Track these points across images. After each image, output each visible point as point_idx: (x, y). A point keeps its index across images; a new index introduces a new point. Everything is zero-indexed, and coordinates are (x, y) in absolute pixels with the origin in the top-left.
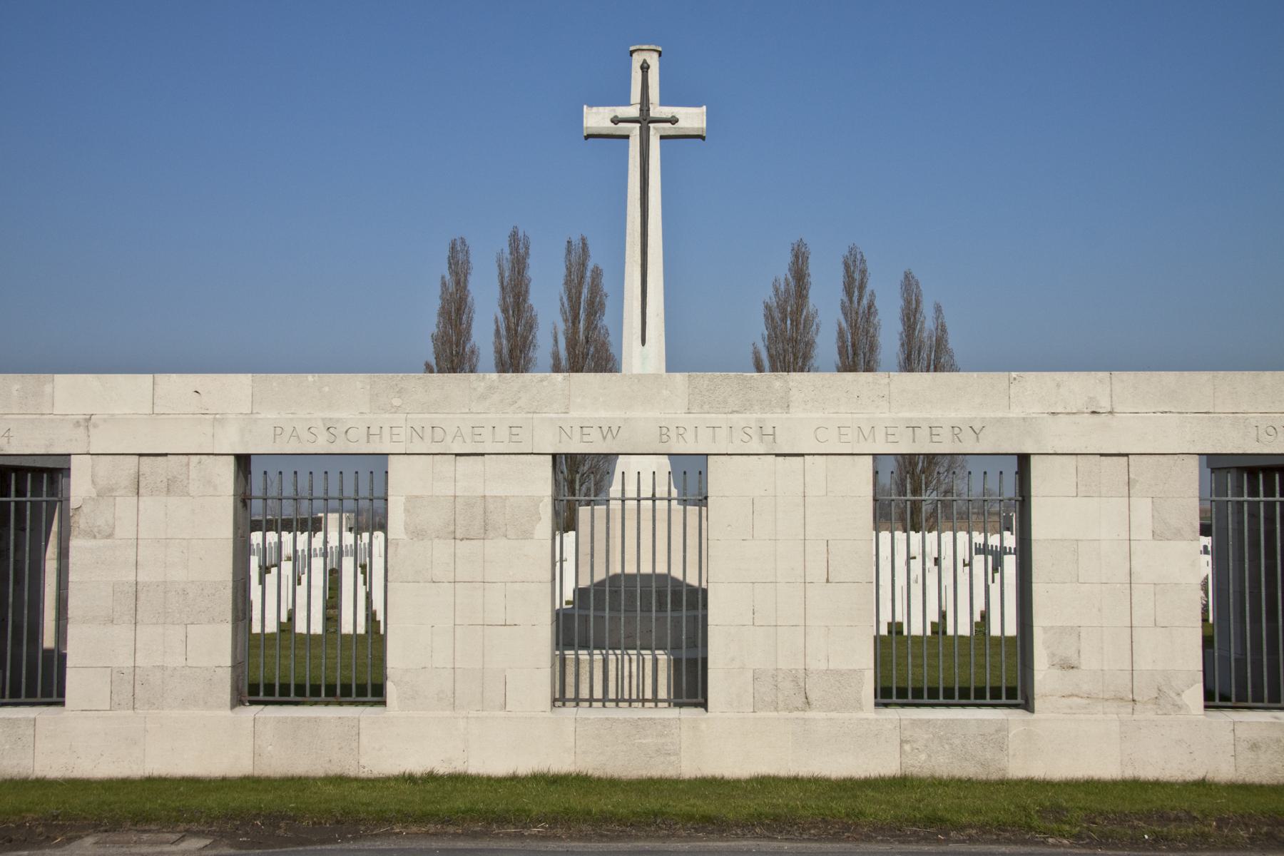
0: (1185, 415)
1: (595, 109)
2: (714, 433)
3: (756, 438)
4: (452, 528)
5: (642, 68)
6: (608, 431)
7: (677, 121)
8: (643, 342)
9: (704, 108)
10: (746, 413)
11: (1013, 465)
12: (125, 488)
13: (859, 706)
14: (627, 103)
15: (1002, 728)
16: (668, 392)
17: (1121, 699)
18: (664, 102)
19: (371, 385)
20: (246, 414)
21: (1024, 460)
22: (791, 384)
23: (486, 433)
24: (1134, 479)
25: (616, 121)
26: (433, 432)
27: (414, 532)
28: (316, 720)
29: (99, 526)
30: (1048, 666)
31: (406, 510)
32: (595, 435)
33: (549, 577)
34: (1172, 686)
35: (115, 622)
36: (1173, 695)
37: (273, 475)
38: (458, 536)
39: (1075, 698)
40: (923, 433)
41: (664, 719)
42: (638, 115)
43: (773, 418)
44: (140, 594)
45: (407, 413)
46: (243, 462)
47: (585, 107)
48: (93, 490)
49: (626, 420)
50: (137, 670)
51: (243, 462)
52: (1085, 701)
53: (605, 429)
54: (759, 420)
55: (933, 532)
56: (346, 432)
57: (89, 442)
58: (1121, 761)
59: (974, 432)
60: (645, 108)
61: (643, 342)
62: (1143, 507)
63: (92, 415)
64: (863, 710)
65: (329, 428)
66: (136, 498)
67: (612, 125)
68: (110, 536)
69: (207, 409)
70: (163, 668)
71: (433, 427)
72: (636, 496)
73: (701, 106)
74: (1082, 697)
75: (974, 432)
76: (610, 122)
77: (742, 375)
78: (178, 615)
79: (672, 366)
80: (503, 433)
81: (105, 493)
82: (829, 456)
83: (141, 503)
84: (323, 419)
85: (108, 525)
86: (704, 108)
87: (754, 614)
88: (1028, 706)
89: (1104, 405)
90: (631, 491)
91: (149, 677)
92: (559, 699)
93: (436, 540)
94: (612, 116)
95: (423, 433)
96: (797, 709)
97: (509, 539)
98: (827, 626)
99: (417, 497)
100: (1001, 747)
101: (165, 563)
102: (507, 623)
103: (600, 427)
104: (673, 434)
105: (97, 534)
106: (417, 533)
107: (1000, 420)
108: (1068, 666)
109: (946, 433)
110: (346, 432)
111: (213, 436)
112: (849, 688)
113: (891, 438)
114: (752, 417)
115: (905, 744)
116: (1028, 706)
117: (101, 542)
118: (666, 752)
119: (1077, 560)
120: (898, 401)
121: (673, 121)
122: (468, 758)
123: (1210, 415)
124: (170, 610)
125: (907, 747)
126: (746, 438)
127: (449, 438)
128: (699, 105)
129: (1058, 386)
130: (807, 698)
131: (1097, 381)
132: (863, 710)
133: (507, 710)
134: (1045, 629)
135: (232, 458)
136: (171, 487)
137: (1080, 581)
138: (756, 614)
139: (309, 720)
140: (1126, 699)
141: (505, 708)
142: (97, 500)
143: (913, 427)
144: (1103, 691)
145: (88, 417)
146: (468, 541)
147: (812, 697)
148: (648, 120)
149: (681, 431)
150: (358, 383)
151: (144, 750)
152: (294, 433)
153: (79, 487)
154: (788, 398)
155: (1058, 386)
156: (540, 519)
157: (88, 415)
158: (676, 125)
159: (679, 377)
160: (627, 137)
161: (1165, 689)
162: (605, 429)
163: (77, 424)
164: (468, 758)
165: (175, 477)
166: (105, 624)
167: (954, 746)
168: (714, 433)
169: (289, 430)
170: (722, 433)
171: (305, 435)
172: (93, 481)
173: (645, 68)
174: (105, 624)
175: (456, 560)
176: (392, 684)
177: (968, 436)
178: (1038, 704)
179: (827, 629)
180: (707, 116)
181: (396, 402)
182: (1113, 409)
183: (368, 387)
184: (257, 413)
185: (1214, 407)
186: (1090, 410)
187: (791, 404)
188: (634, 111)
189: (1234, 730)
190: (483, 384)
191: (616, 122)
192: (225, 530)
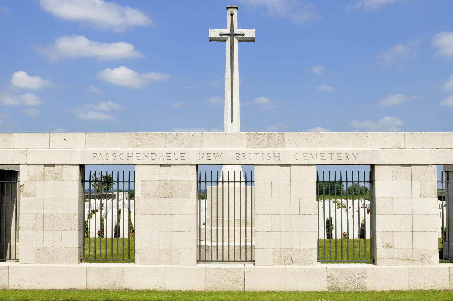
0: (432, 149)
1: (213, 30)
2: (331, 155)
3: (272, 158)
4: (159, 193)
5: (231, 14)
6: (217, 155)
7: (244, 35)
8: (232, 121)
9: (254, 29)
10: (268, 148)
11: (369, 169)
12: (39, 177)
13: (311, 263)
14: (226, 28)
15: (365, 271)
16: (239, 140)
17: (409, 260)
18: (239, 28)
19: (129, 137)
20: (83, 148)
21: (373, 166)
22: (285, 137)
23: (172, 156)
24: (413, 174)
25: (221, 35)
26: (152, 155)
27: (145, 195)
28: (109, 268)
29: (30, 192)
30: (382, 247)
31: (142, 186)
32: (212, 157)
33: (195, 212)
34: (427, 254)
35: (36, 230)
36: (428, 258)
37: (93, 173)
38: (161, 196)
39: (392, 259)
40: (335, 156)
41: (238, 268)
42: (230, 33)
43: (279, 149)
44: (45, 219)
45: (143, 148)
46: (82, 167)
47: (210, 29)
48: (28, 178)
49: (223, 151)
50: (44, 248)
51: (82, 167)
52: (395, 261)
53: (216, 154)
54: (273, 151)
55: (204, 200)
56: (120, 155)
57: (27, 159)
58: (409, 283)
59: (354, 156)
60: (232, 30)
61: (232, 121)
62: (416, 185)
63: (28, 149)
64: (313, 265)
65: (113, 154)
66: (43, 181)
67: (220, 36)
68: (34, 196)
69: (69, 147)
70: (53, 247)
71: (152, 154)
72: (234, 181)
73: (253, 29)
74: (394, 259)
75: (354, 156)
76: (219, 35)
77: (267, 133)
78: (59, 227)
79: (242, 130)
80: (178, 156)
81: (32, 179)
82: (154, 166)
83: (45, 183)
84: (111, 150)
85: (34, 192)
86: (254, 29)
87: (272, 227)
88: (373, 262)
89: (402, 145)
90: (226, 179)
91: (48, 251)
92: (199, 261)
93: (153, 198)
94: (219, 33)
95: (148, 156)
96: (288, 264)
97: (180, 197)
98: (299, 232)
99: (146, 181)
100: (365, 279)
101: (54, 207)
102: (180, 231)
103: (214, 154)
104: (241, 156)
105: (29, 195)
106: (146, 195)
107: (363, 151)
108: (388, 246)
109: (343, 156)
110: (120, 155)
111: (71, 157)
112: (307, 256)
113: (323, 158)
114: (271, 149)
115: (328, 278)
116: (373, 262)
117: (31, 198)
118: (239, 281)
119: (393, 205)
120: (325, 144)
121: (242, 35)
122: (165, 283)
123: (441, 149)
124: (56, 225)
125: (329, 279)
126: (269, 158)
127: (158, 158)
128: (252, 28)
129: (385, 137)
130: (292, 260)
131: (400, 136)
132: (313, 265)
133: (180, 264)
134: (381, 232)
135: (78, 167)
136: (56, 177)
137: (394, 214)
138: (272, 227)
139: (106, 268)
140: (410, 259)
141: (179, 264)
142: (29, 182)
143: (331, 154)
144: (402, 256)
145: (26, 149)
146: (165, 198)
147: (294, 259)
148: (233, 34)
149: (244, 155)
150: (124, 136)
151: (47, 279)
152: (101, 156)
153: (22, 178)
154: (285, 142)
155: (385, 137)
156: (192, 189)
157: (26, 149)
158: (244, 37)
159: (243, 133)
160: (226, 41)
161: (424, 255)
162: (216, 154)
163: (22, 152)
164: (165, 283)
165: (57, 173)
166: (32, 230)
167: (347, 278)
168: (331, 155)
169: (99, 154)
170: (141, 156)
171: (105, 157)
172: (28, 174)
173: (232, 14)
174: (32, 230)
175: (161, 206)
176: (137, 254)
177: (351, 157)
178: (378, 262)
179: (299, 233)
180: (255, 33)
181: (138, 144)
182: (405, 147)
183: (128, 138)
184: (87, 148)
185: (442, 146)
186: (397, 147)
187: (285, 144)
188: (228, 31)
189: (449, 271)
190: (170, 137)
191: (221, 35)
192: (378, 184)
